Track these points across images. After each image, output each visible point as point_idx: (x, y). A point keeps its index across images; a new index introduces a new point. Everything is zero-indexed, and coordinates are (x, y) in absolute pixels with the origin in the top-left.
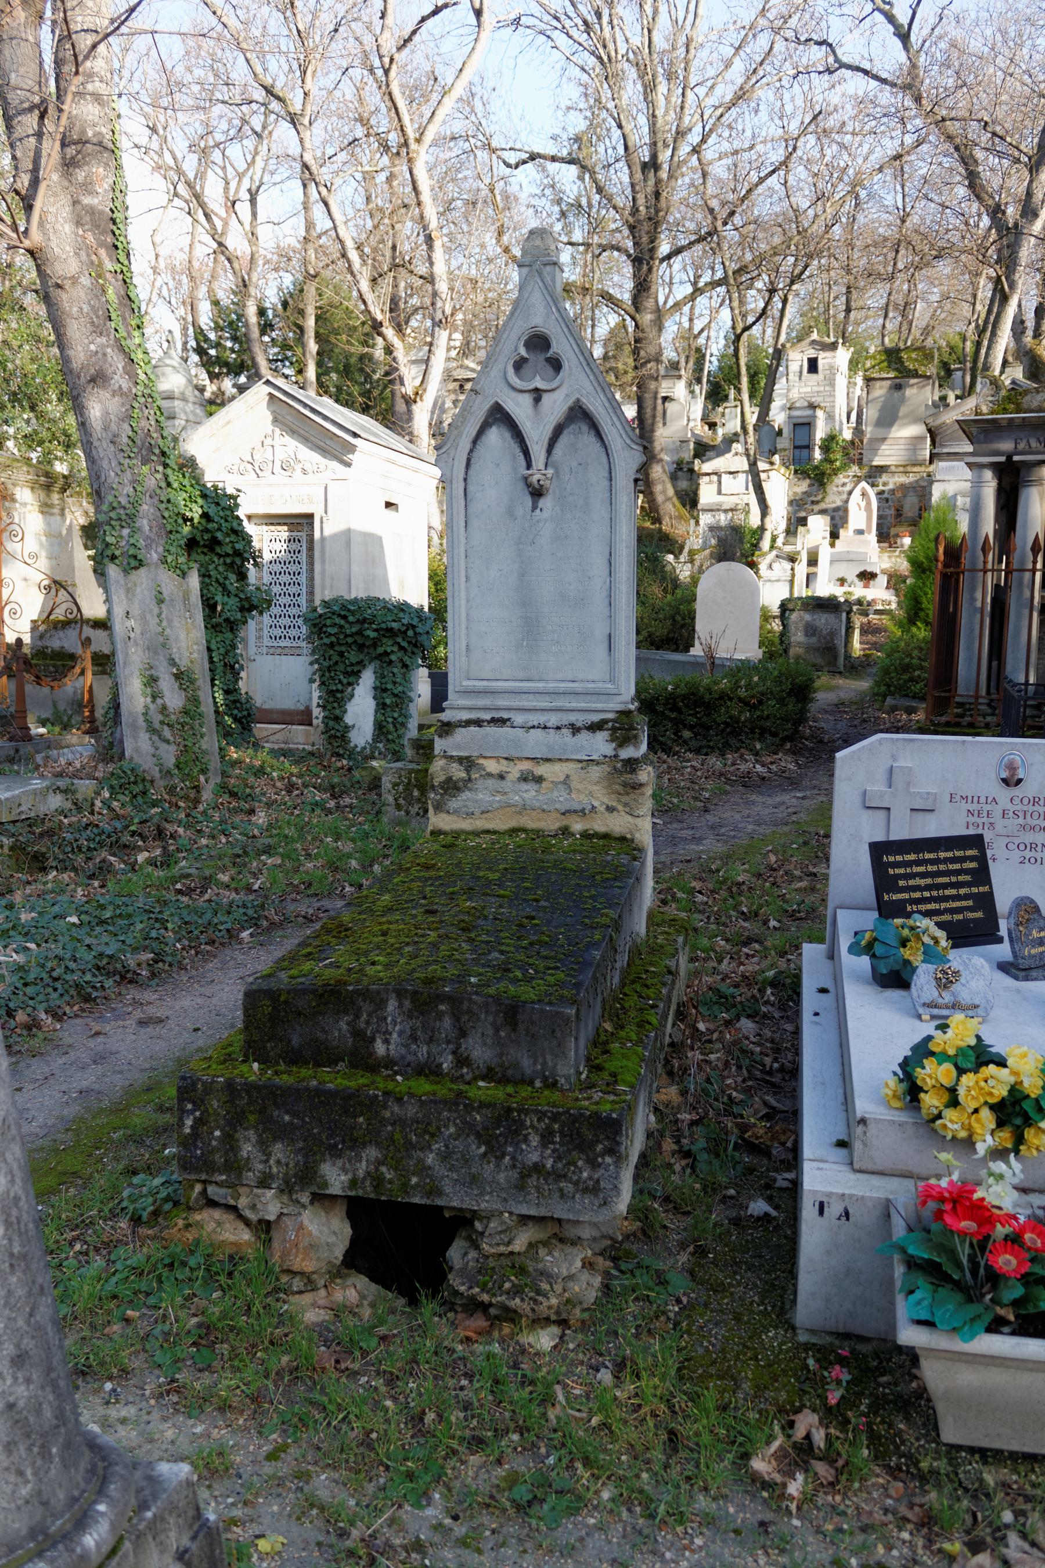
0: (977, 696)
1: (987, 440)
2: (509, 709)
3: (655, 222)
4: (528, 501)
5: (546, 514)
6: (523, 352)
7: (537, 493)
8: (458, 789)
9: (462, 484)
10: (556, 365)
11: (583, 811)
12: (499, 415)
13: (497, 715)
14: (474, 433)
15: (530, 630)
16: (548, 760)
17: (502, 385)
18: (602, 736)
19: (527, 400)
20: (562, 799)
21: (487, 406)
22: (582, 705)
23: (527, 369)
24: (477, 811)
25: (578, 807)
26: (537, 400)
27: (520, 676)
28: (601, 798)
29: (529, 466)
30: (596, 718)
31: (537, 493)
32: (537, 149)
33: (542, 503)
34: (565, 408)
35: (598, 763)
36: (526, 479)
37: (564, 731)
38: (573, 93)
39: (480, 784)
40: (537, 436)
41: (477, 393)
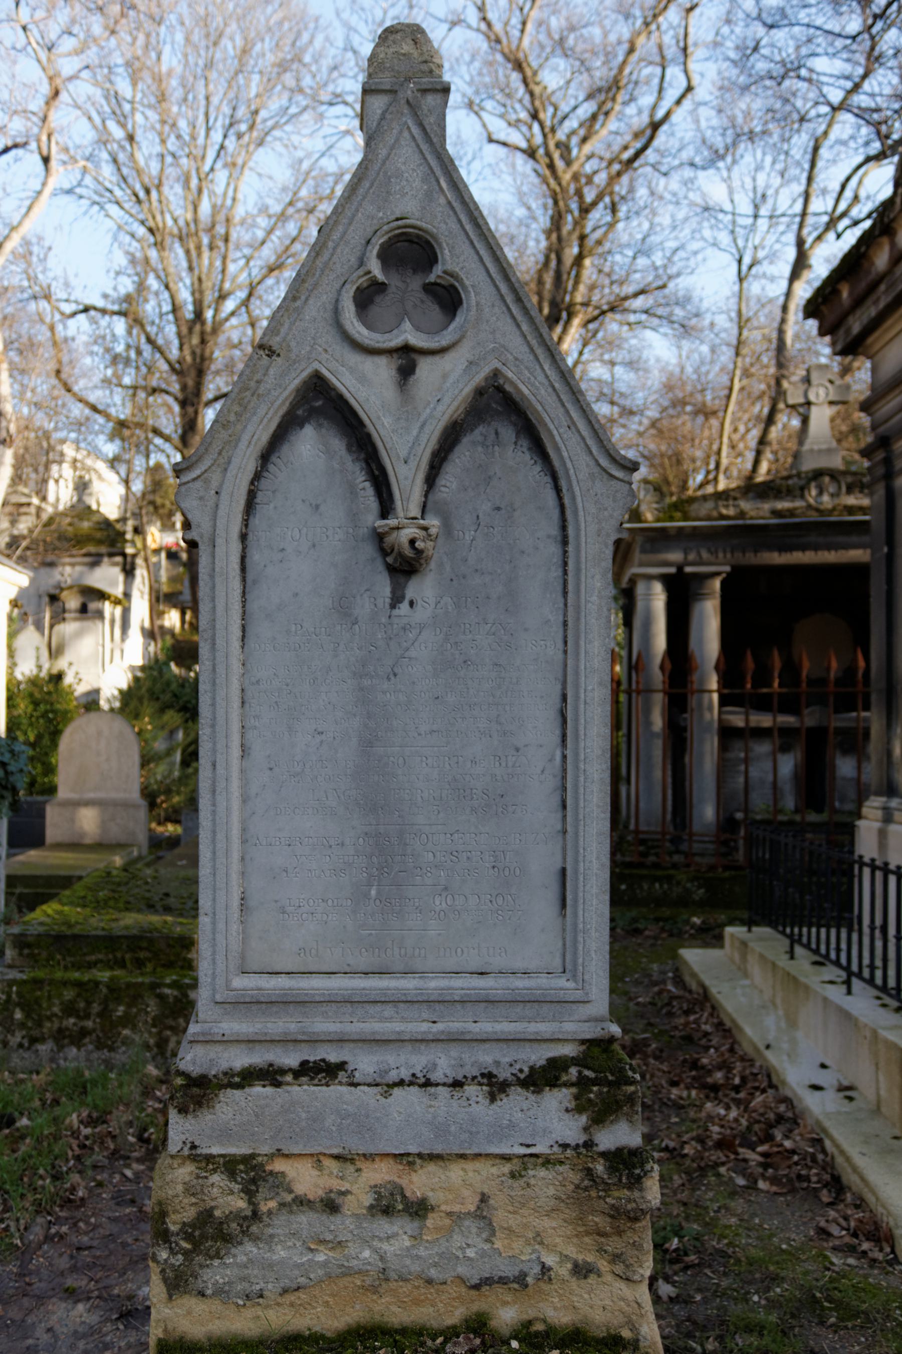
0: (664, 833)
1: (654, 551)
2: (341, 1041)
3: (200, 373)
4: (384, 586)
5: (421, 614)
6: (376, 268)
7: (403, 566)
8: (227, 1239)
9: (235, 547)
10: (448, 298)
11: (521, 1279)
12: (321, 402)
13: (314, 1055)
14: (264, 437)
15: (385, 862)
16: (433, 1157)
18: (556, 1100)
19: (383, 371)
20: (471, 1252)
21: (295, 381)
22: (505, 1028)
23: (382, 307)
24: (271, 1289)
25: (510, 1271)
26: (406, 372)
27: (363, 961)
28: (561, 1246)
29: (386, 508)
30: (538, 1056)
31: (403, 566)
32: (89, 302)
33: (412, 589)
34: (468, 389)
35: (547, 1162)
36: (379, 537)
37: (471, 1090)
38: (122, 260)
39: (279, 1225)
41: (272, 353)
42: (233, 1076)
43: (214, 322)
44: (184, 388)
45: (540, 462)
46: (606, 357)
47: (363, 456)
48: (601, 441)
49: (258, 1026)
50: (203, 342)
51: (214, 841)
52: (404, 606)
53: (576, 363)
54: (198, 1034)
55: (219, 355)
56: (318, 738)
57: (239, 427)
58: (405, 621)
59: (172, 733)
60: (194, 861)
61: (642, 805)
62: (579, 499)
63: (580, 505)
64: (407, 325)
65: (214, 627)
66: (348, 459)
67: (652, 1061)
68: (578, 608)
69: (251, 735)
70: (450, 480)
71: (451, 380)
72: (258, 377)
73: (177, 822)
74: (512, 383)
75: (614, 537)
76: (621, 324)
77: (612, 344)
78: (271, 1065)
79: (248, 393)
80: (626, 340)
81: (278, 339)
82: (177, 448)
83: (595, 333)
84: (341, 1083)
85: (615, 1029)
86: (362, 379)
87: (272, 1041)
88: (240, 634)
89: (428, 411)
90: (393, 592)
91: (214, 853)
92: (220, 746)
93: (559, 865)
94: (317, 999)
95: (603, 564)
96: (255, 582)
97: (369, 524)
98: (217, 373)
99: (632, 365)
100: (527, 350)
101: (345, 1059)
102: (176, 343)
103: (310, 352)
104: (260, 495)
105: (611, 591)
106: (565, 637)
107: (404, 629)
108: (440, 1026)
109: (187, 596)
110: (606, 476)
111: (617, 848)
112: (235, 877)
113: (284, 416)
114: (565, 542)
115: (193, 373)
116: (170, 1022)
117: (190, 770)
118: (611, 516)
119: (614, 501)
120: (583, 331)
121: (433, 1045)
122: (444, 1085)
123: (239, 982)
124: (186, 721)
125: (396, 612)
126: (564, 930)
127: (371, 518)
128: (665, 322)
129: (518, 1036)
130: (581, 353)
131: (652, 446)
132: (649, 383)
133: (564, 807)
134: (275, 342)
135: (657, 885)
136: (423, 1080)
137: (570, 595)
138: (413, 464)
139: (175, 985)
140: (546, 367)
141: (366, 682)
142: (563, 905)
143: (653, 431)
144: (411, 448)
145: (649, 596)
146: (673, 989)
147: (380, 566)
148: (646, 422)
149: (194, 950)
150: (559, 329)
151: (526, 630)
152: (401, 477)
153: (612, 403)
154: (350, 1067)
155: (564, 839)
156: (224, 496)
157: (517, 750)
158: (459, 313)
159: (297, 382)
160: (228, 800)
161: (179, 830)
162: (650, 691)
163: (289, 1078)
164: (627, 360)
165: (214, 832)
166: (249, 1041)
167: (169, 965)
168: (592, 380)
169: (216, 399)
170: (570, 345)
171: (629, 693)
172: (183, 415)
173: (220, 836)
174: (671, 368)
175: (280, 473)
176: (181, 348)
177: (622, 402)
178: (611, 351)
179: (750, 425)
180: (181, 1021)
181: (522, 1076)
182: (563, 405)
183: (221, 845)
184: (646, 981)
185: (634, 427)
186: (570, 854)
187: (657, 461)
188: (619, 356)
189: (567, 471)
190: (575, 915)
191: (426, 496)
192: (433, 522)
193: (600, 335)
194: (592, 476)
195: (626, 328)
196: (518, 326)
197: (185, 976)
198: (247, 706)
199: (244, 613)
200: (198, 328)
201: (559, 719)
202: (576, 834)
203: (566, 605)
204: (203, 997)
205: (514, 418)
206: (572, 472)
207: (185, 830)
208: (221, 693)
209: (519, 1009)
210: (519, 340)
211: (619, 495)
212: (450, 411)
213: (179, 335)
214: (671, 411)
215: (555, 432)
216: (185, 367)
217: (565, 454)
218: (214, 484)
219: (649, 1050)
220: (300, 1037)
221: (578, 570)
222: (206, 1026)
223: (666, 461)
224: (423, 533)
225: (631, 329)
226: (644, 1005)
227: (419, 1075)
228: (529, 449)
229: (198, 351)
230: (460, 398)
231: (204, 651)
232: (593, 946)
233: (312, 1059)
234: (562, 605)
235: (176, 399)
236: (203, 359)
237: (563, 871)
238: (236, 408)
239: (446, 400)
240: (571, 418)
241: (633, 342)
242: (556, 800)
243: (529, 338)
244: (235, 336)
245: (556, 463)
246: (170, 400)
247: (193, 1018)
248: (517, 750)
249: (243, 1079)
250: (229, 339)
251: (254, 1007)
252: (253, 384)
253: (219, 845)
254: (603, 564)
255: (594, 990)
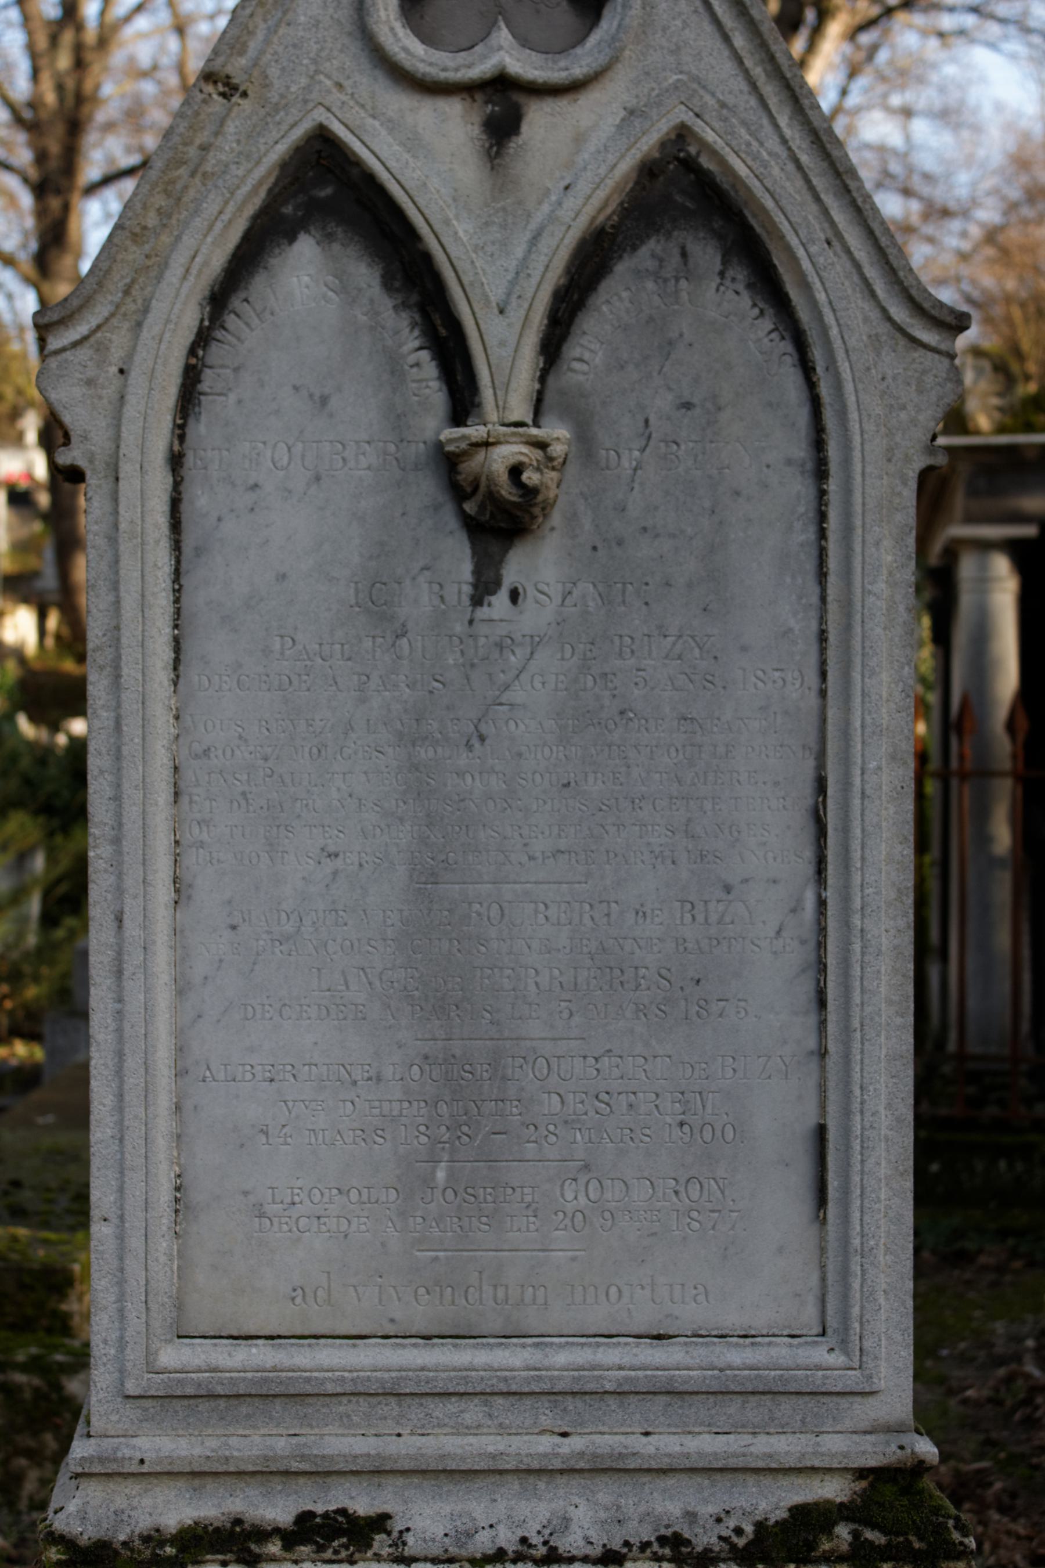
2: (377, 1472)
4: (459, 561)
5: (536, 616)
7: (498, 520)
9: (160, 481)
12: (330, 191)
14: (216, 259)
15: (464, 1111)
17: (346, 60)
19: (454, 126)
21: (278, 146)
22: (706, 1445)
26: (501, 130)
27: (420, 1313)
29: (463, 403)
31: (498, 520)
33: (516, 567)
34: (627, 165)
36: (448, 462)
40: (499, 276)
41: (230, 89)
42: (162, 1544)
43: (102, 25)
44: (41, 157)
45: (770, 311)
46: (896, 100)
47: (415, 298)
48: (893, 271)
49: (213, 1443)
50: (80, 64)
51: (119, 1072)
52: (500, 600)
53: (837, 110)
54: (90, 1460)
55: (111, 91)
56: (329, 866)
57: (165, 239)
58: (501, 630)
59: (23, 858)
60: (78, 1116)
61: (972, 1003)
62: (849, 387)
63: (851, 400)
64: (503, 35)
65: (116, 643)
66: (386, 304)
67: (995, 1516)
68: (847, 605)
69: (191, 859)
70: (590, 347)
71: (593, 144)
72: (202, 137)
73: (32, 1036)
74: (714, 153)
75: (920, 462)
76: (924, 33)
77: (906, 74)
78: (238, 1521)
79: (183, 171)
80: (934, 66)
81: (243, 61)
82: (27, 280)
83: (873, 50)
84: (378, 1558)
85: (926, 1448)
86: (413, 143)
87: (240, 1474)
88: (168, 655)
89: (546, 208)
90: (477, 572)
91: (120, 1096)
92: (131, 882)
93: (812, 1120)
94: (330, 1388)
95: (899, 517)
96: (199, 551)
97: (429, 435)
98: (109, 127)
99: (948, 116)
100: (744, 86)
101: (387, 1508)
102: (23, 66)
103: (308, 89)
104: (208, 375)
105: (908, 574)
106: (823, 663)
107: (500, 646)
108: (576, 1443)
109: (49, 580)
110: (902, 342)
111: (926, 1086)
112: (162, 1144)
113: (256, 218)
114: (821, 472)
115: (60, 129)
116: (26, 1440)
117: (60, 933)
118: (914, 422)
119: (920, 391)
120: (847, 48)
121: (561, 1480)
122: (585, 1559)
123: (171, 1356)
124: (51, 834)
125: (483, 612)
126: (823, 1250)
127: (431, 423)
128: (1012, 30)
129: (732, 1463)
130: (844, 92)
131: (988, 281)
132: (981, 153)
133: (822, 1003)
134: (236, 67)
135: (1003, 1165)
136: (543, 1550)
137: (832, 579)
138: (516, 314)
139: (34, 1365)
140: (783, 121)
141: (425, 753)
142: (822, 1200)
143: (990, 251)
144: (513, 283)
145: (984, 582)
146: (1036, 1372)
147: (450, 520)
148: (975, 231)
149: (73, 1296)
150: (798, 46)
151: (744, 649)
152: (491, 341)
153: (907, 192)
154: (397, 1525)
155: (823, 1068)
156: (137, 378)
157: (728, 889)
158: (607, 12)
159: (282, 149)
160: (148, 990)
161: (39, 1053)
162: (984, 773)
163: (274, 1547)
164: (938, 103)
165: (120, 1055)
166: (194, 1474)
167: (23, 1326)
168: (868, 146)
169: (108, 180)
170: (823, 74)
171: (944, 777)
172: (40, 213)
173: (133, 1062)
174: (1024, 124)
175: (247, 332)
176: (35, 74)
177: (926, 190)
178: (903, 87)
179: (966, 287)
180: (50, 1441)
181: (741, 1542)
182: (817, 199)
183: (133, 1080)
184: (982, 1354)
185: (953, 242)
186: (834, 1097)
187: (998, 311)
188: (922, 97)
189: (824, 330)
190: (845, 1219)
191: (543, 379)
192: (557, 432)
193: (883, 56)
194: (875, 339)
195: (933, 43)
196: (726, 39)
197: (56, 1348)
198: (185, 800)
199: (178, 612)
200: (68, 37)
201: (811, 829)
202: (847, 1057)
203: (823, 599)
204: (99, 1390)
205: (717, 224)
206: (834, 332)
207: (51, 1054)
208: (132, 774)
209: (733, 1407)
210: (729, 67)
211: (929, 379)
212: (590, 210)
213: (31, 49)
214: (1027, 212)
215: (801, 253)
216: (44, 115)
217: (821, 297)
218: (116, 354)
219: (990, 1494)
220: (295, 1466)
221: (848, 529)
222: (108, 1444)
223: (1017, 313)
224: (537, 454)
225: (945, 45)
226: (977, 1404)
227: (535, 1540)
228: (749, 286)
229: (70, 84)
230: (610, 183)
231: (97, 689)
232: (882, 1282)
233: (320, 1509)
234: (815, 599)
235: (26, 180)
236: (80, 99)
237: (821, 1132)
238: (160, 200)
239: (583, 187)
240: (832, 223)
241: (950, 70)
242: (806, 988)
243: (748, 63)
244: (144, 54)
245: (804, 315)
246: (12, 182)
247: (80, 1429)
248: (728, 889)
249: (183, 1549)
250: (132, 60)
251: (204, 1406)
252: (192, 152)
253: (130, 1081)
254: (899, 517)
255: (884, 1369)
